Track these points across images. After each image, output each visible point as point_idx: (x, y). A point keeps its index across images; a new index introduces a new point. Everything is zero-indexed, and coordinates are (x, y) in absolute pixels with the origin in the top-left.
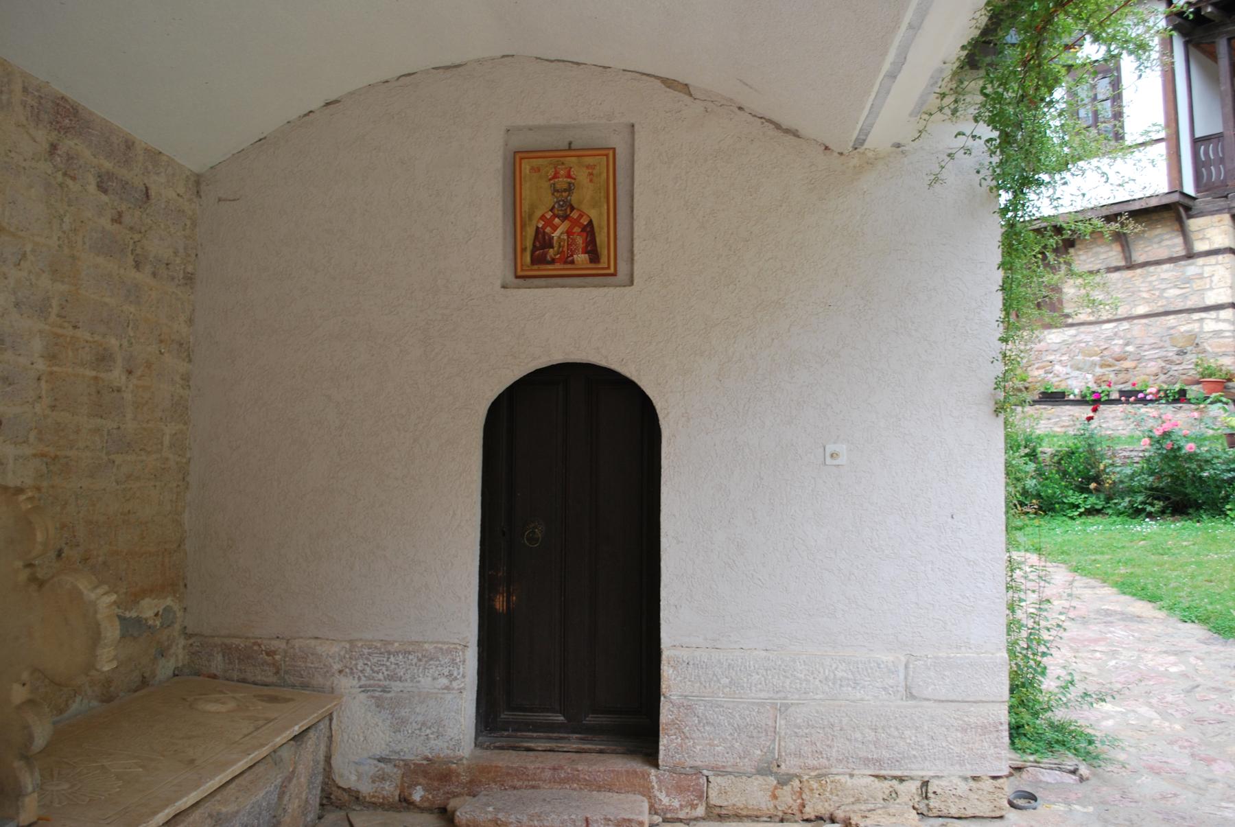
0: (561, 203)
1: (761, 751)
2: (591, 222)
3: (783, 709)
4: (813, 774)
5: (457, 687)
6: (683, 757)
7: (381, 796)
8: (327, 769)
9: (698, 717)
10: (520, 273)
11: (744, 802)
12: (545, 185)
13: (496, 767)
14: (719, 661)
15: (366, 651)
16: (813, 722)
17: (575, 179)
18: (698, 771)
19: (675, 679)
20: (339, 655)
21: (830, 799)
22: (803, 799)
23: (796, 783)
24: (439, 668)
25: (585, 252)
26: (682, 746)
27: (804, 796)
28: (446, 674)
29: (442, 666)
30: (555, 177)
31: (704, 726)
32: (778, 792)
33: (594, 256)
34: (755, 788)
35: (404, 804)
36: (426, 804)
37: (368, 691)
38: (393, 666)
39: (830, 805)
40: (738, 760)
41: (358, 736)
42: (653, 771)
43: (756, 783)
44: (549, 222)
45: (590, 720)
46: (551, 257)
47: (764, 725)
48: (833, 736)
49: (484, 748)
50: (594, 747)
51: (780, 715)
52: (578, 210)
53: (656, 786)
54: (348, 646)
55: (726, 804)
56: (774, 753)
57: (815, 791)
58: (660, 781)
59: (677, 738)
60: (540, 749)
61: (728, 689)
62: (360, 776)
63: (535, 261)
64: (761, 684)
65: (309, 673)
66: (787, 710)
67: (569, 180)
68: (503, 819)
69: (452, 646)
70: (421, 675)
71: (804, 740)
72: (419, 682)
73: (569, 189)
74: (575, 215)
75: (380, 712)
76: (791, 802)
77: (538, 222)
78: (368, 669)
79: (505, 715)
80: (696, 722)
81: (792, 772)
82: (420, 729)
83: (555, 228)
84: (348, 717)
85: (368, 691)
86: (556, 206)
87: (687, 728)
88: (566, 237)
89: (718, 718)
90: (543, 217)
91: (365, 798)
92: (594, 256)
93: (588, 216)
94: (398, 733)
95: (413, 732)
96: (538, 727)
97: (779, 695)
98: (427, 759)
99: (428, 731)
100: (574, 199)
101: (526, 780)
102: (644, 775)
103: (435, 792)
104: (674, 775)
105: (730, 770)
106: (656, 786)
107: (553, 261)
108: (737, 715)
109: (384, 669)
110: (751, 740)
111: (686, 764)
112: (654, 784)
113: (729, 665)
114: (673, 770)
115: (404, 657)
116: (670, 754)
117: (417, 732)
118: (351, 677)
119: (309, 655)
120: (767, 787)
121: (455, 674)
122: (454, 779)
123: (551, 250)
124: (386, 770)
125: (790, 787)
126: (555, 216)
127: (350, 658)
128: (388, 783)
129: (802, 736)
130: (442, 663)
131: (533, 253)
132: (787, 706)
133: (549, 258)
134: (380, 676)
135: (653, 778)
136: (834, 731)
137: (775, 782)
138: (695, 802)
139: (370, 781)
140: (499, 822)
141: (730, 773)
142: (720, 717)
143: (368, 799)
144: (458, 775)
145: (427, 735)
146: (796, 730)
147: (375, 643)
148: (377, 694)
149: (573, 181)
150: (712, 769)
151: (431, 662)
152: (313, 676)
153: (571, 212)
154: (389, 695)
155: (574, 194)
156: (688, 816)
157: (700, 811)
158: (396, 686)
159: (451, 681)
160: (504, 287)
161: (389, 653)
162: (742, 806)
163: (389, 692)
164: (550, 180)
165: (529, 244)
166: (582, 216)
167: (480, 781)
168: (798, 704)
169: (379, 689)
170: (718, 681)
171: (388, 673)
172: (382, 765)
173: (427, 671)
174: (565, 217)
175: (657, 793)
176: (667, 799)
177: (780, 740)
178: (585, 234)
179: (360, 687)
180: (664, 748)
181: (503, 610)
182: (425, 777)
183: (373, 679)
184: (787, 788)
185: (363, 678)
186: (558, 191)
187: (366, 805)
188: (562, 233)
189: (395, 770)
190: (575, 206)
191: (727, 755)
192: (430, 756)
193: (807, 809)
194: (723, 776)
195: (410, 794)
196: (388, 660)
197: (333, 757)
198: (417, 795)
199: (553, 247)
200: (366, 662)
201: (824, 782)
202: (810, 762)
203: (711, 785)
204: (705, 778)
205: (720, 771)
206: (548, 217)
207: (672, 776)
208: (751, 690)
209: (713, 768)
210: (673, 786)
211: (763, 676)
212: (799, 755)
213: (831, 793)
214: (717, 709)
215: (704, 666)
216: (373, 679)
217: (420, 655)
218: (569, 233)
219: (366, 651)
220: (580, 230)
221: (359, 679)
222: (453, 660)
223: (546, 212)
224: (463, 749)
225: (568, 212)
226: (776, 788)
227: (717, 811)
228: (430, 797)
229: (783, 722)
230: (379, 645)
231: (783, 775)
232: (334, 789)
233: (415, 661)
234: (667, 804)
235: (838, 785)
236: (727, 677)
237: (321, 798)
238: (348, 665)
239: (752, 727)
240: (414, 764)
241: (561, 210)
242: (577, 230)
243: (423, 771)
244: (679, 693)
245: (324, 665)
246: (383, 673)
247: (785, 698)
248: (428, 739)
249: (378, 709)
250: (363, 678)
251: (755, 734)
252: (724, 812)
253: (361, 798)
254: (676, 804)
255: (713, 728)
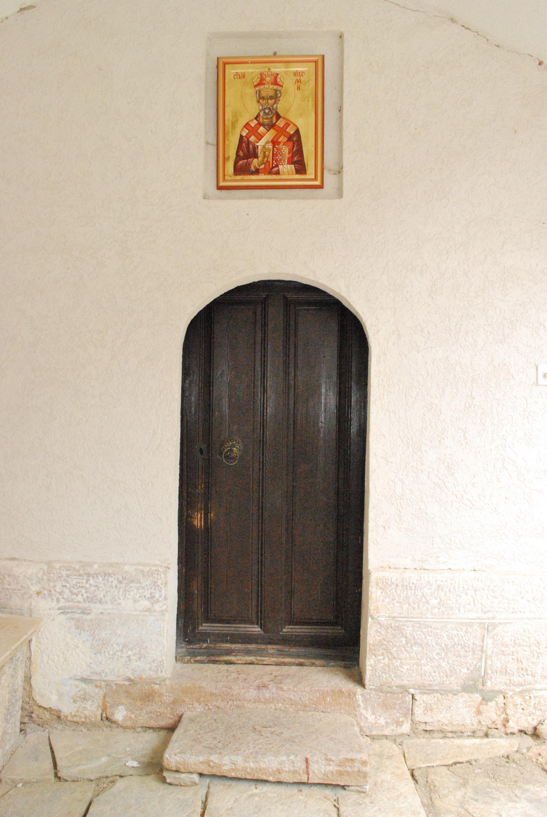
0: (267, 111)
1: (468, 669)
2: (297, 132)
3: (490, 628)
4: (518, 689)
5: (158, 610)
6: (390, 676)
7: (83, 716)
8: (28, 688)
9: (406, 638)
10: (222, 184)
11: (449, 718)
12: (251, 91)
13: (200, 687)
14: (429, 582)
15: (64, 573)
16: (520, 641)
17: (282, 86)
18: (404, 689)
19: (383, 601)
20: (37, 576)
21: (533, 714)
22: (507, 714)
23: (500, 699)
24: (141, 591)
25: (290, 162)
26: (389, 667)
27: (508, 712)
28: (147, 596)
29: (143, 588)
30: (261, 83)
31: (411, 647)
32: (483, 708)
33: (301, 168)
34: (461, 705)
35: (107, 723)
36: (129, 723)
37: (67, 613)
38: (93, 588)
39: (533, 719)
40: (445, 679)
41: (58, 656)
42: (359, 690)
43: (461, 700)
44: (253, 131)
45: (287, 630)
46: (255, 167)
47: (471, 646)
48: (539, 653)
49: (184, 663)
50: (293, 660)
51: (488, 634)
52: (284, 118)
53: (362, 705)
54: (45, 567)
55: (431, 720)
56: (480, 671)
57: (519, 706)
58: (365, 700)
59: (384, 659)
60: (239, 662)
61: (436, 610)
62: (60, 695)
63: (239, 170)
64: (469, 604)
65: (7, 595)
66: (494, 629)
67: (275, 87)
68: (217, 761)
69: (154, 568)
70: (121, 598)
71: (510, 658)
72: (120, 604)
73: (276, 97)
74: (281, 123)
75: (80, 634)
76: (495, 717)
77: (242, 130)
78: (67, 591)
79: (205, 627)
80: (404, 642)
81: (497, 688)
82: (122, 651)
83: (260, 137)
84: (47, 639)
85: (67, 613)
86: (261, 114)
87: (395, 649)
88: (271, 147)
89: (426, 638)
90: (247, 126)
91: (66, 717)
92: (301, 168)
93: (295, 125)
94: (99, 655)
95: (114, 654)
96: (234, 638)
97: (487, 615)
98: (130, 680)
99: (130, 653)
100: (281, 107)
101: (230, 700)
102: (350, 695)
103: (138, 712)
104: (380, 694)
105: (436, 688)
106: (362, 705)
107: (257, 172)
108: (445, 635)
109: (83, 591)
110: (458, 658)
111: (393, 683)
112: (360, 702)
113: (439, 586)
114: (379, 689)
115: (104, 580)
116: (377, 674)
117: (119, 653)
118: (50, 599)
119: (6, 577)
120: (472, 703)
121: (157, 596)
122: (157, 699)
123: (255, 160)
124: (87, 690)
125: (495, 702)
126: (260, 124)
127: (49, 580)
128: (90, 703)
129: (509, 654)
130: (143, 585)
131: (236, 163)
132: (494, 626)
133: (252, 168)
134: (80, 598)
135: (359, 697)
136: (539, 649)
137: (480, 698)
138: (401, 719)
139: (72, 700)
140: (212, 764)
141: (437, 691)
142: (428, 637)
143: (69, 718)
144: (161, 695)
145: (129, 657)
146: (503, 649)
147: (73, 565)
148: (77, 616)
149: (279, 88)
150: (419, 688)
151: (132, 585)
152: (11, 597)
153: (277, 120)
154: (88, 617)
155: (281, 102)
156: (394, 733)
157: (406, 728)
158: (96, 608)
159: (153, 604)
160: (205, 197)
161: (88, 575)
162: (447, 722)
163: (89, 614)
164: (255, 86)
165: (232, 153)
166: (289, 125)
167: (184, 701)
168: (505, 623)
169: (79, 611)
170: (427, 602)
171: (88, 594)
172: (83, 685)
173: (127, 593)
174: (272, 126)
175: (364, 712)
176: (373, 717)
177: (486, 659)
178: (291, 144)
179: (59, 609)
180: (370, 668)
181: (201, 525)
182: (127, 697)
183: (72, 600)
184: (492, 704)
185: (62, 600)
186: (263, 98)
187: (68, 724)
188: (266, 143)
189: (97, 690)
190: (281, 114)
191: (433, 674)
192: (132, 677)
193: (511, 724)
194: (429, 694)
195: (113, 714)
196: (87, 582)
197: (33, 678)
198: (120, 714)
199: (256, 156)
200: (64, 584)
201: (527, 698)
202: (515, 679)
203: (417, 703)
204: (411, 696)
205: (427, 690)
206: (253, 126)
207: (378, 695)
208: (459, 610)
209: (419, 687)
210: (378, 704)
211: (472, 596)
212: (505, 672)
213: (535, 708)
214: (425, 630)
215: (413, 588)
216: (72, 600)
217: (120, 578)
218: (274, 142)
219: (64, 573)
220: (286, 139)
221: (58, 600)
222: (155, 582)
223: (252, 120)
224: (166, 671)
225: (274, 120)
226: (481, 704)
227: (422, 727)
228: (133, 716)
229: (490, 641)
230: (77, 567)
231: (488, 692)
232: (35, 708)
233: (115, 583)
234: (373, 722)
235: (542, 700)
236: (436, 598)
237: (22, 716)
238: (46, 586)
239: (459, 647)
240: (116, 684)
241: (267, 118)
242: (283, 139)
243: (125, 692)
244: (387, 615)
245: (22, 587)
246: (82, 595)
247: (493, 618)
248: (129, 660)
249: (78, 631)
250: (62, 600)
251: (462, 653)
252: (428, 728)
253: (63, 717)
254: (382, 721)
255: (420, 649)
